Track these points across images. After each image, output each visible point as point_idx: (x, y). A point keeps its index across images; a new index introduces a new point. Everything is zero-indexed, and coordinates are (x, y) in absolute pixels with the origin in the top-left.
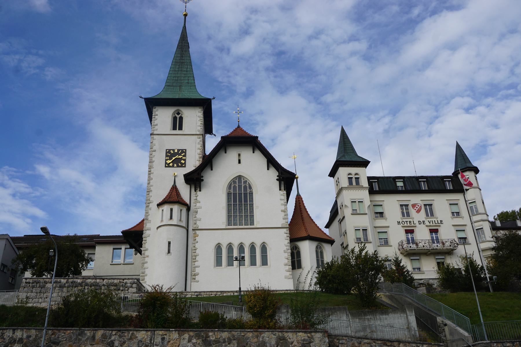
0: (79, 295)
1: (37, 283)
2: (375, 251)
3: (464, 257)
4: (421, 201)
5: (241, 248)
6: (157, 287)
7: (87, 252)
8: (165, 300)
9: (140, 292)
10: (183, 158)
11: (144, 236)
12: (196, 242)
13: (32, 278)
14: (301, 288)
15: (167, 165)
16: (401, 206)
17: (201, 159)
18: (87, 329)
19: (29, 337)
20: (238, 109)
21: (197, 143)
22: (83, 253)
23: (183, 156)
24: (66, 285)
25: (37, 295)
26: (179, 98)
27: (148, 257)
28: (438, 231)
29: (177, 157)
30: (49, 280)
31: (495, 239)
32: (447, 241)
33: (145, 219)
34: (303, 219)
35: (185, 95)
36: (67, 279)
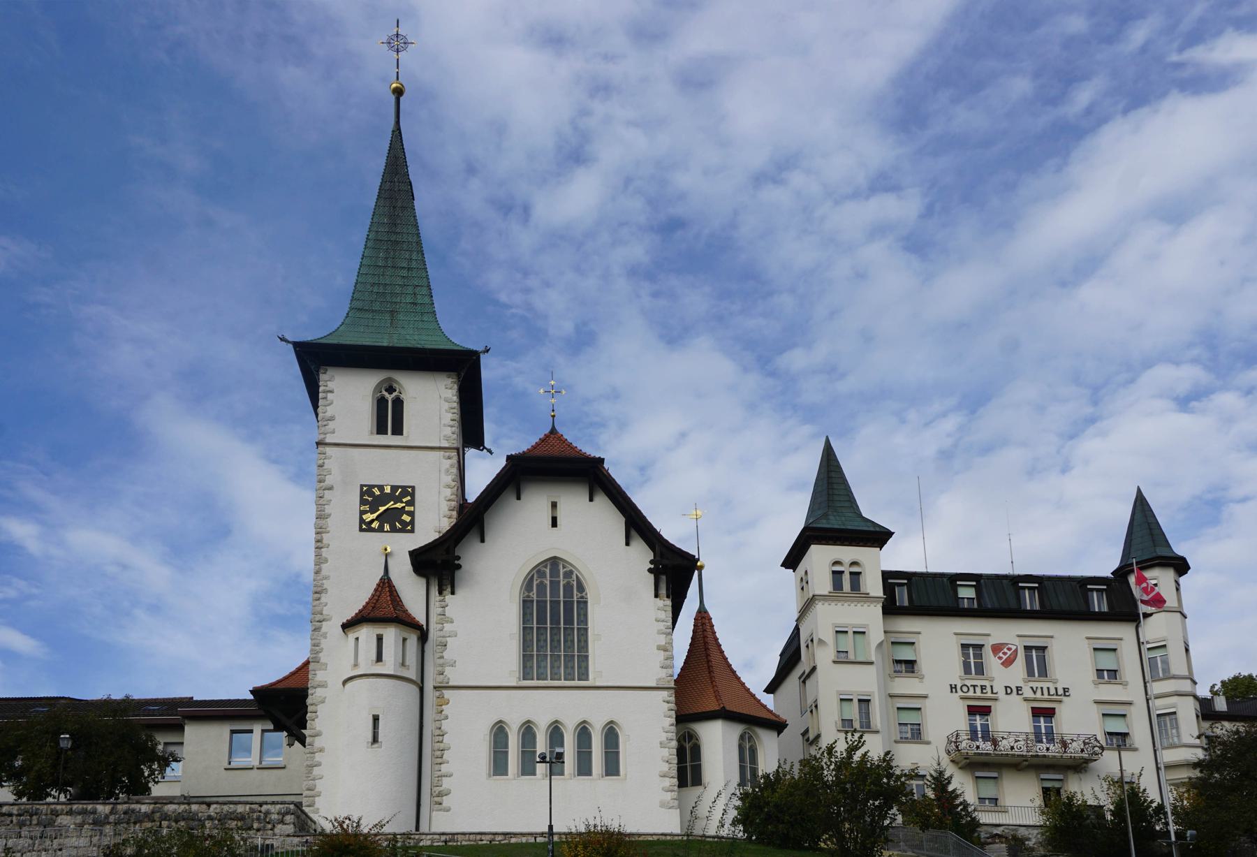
0: (146, 841)
1: (31, 816)
2: (887, 753)
3: (1116, 780)
4: (1018, 638)
5: (556, 733)
6: (347, 822)
7: (161, 739)
8: (368, 851)
9: (304, 834)
11: (309, 701)
12: (443, 717)
13: (17, 802)
14: (698, 831)
15: (364, 527)
16: (963, 645)
17: (455, 514)
20: (553, 383)
21: (443, 471)
22: (151, 741)
23: (405, 502)
24: (112, 818)
25: (34, 844)
26: (391, 345)
27: (321, 750)
28: (1054, 714)
29: (390, 505)
30: (64, 807)
31: (1204, 740)
32: (1075, 739)
33: (310, 660)
34: (713, 679)
35: (406, 339)
36: (112, 804)
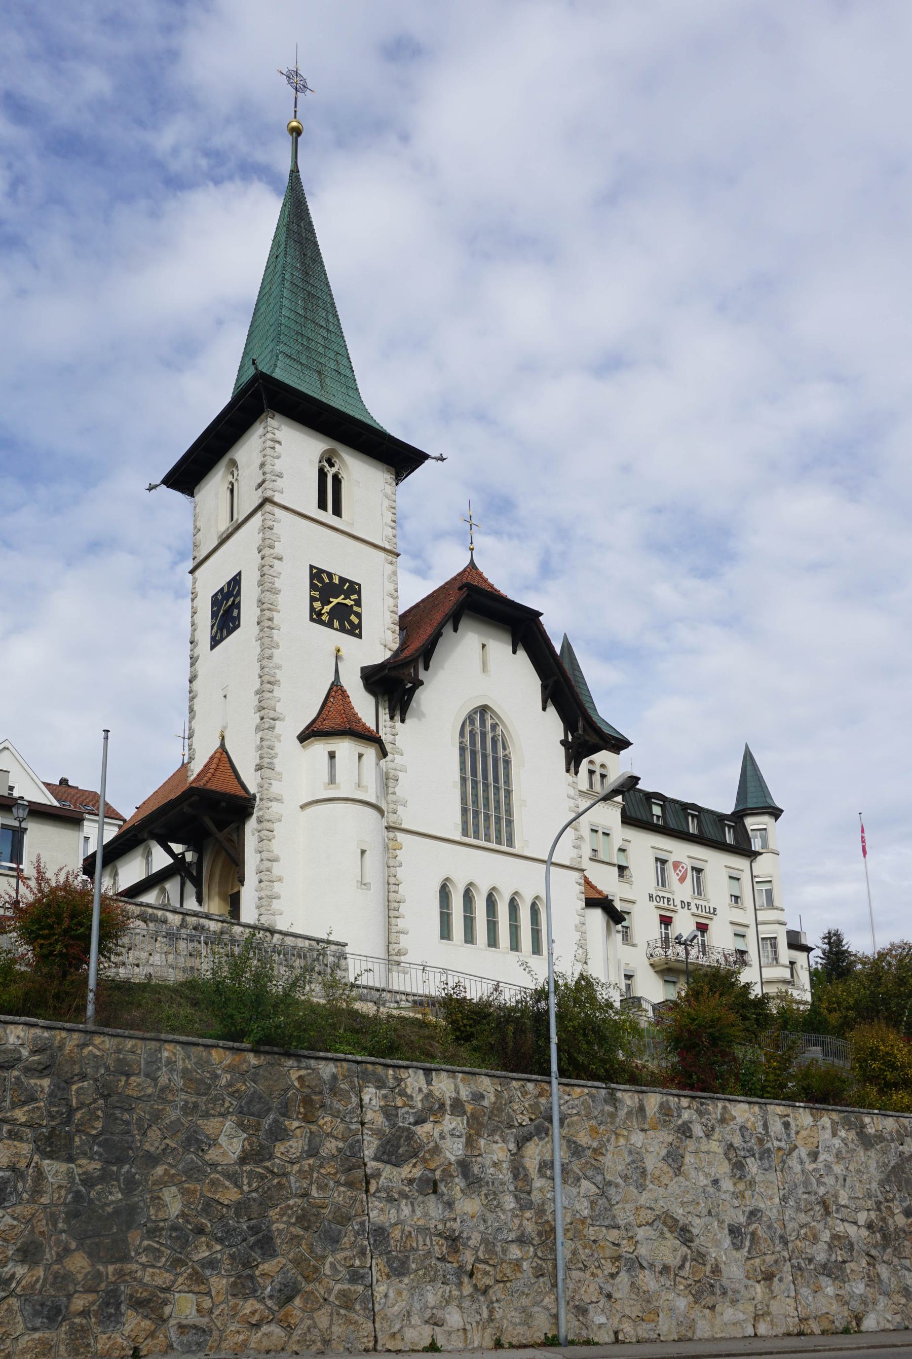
18: (622, 1087)
19: (478, 1097)
21: (386, 576)
28: (671, 922)
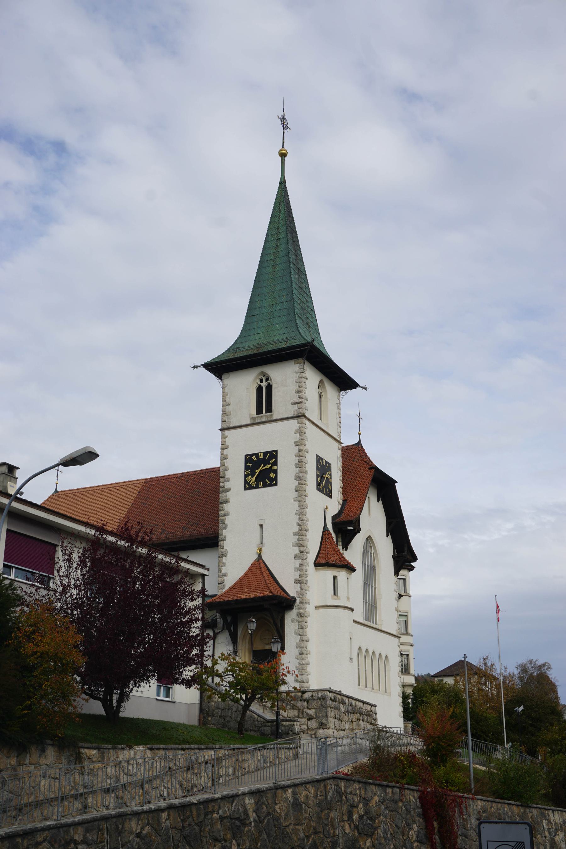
10: (273, 468)
